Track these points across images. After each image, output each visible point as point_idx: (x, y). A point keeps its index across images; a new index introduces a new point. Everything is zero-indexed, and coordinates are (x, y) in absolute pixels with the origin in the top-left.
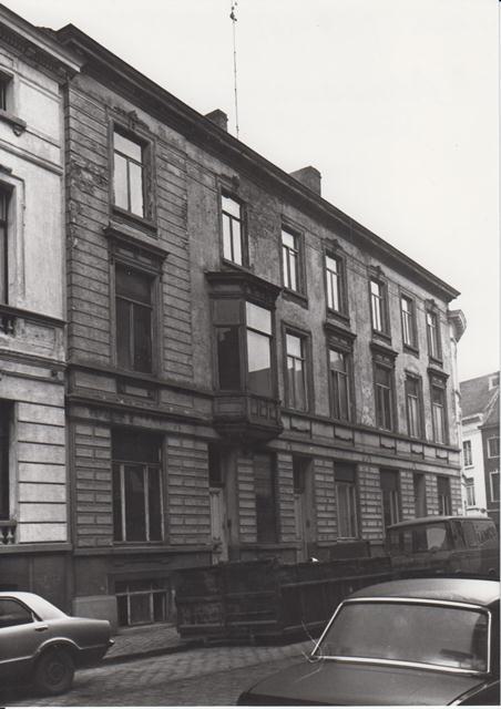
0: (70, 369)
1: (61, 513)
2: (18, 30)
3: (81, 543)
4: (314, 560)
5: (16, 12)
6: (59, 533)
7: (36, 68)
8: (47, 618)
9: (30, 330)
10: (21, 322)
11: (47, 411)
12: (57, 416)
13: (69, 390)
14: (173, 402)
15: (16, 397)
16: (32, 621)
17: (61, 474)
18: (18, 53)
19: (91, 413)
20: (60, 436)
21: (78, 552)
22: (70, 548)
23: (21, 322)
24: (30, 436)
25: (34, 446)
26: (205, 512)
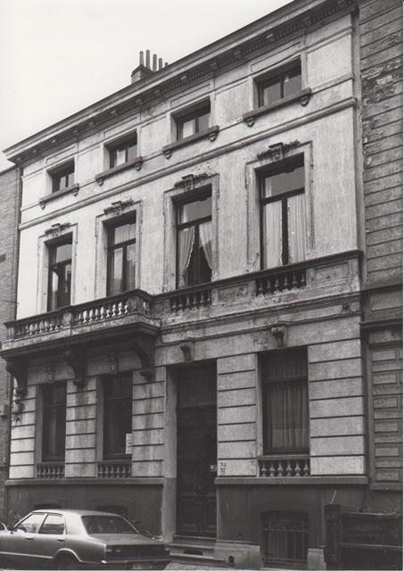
0: (364, 296)
1: (358, 445)
2: (287, 18)
3: (380, 477)
4: (104, 562)
5: (266, 14)
6: (356, 466)
7: (324, 25)
8: (71, 533)
9: (321, 275)
10: (311, 272)
11: (339, 347)
12: (354, 348)
13: (363, 319)
14: (104, 324)
15: (306, 342)
16: (62, 533)
17: (357, 406)
18: (302, 32)
19: (393, 335)
20: (355, 368)
21: (375, 486)
22: (363, 480)
23: (311, 272)
24: (321, 375)
25: (325, 383)
26: (301, 456)
